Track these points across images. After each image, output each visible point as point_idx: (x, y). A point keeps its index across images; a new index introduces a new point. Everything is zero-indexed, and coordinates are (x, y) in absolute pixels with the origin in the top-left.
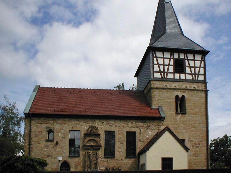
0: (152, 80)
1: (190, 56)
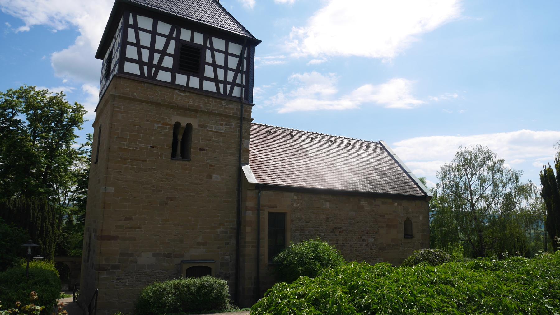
0: (242, 106)
1: (219, 44)
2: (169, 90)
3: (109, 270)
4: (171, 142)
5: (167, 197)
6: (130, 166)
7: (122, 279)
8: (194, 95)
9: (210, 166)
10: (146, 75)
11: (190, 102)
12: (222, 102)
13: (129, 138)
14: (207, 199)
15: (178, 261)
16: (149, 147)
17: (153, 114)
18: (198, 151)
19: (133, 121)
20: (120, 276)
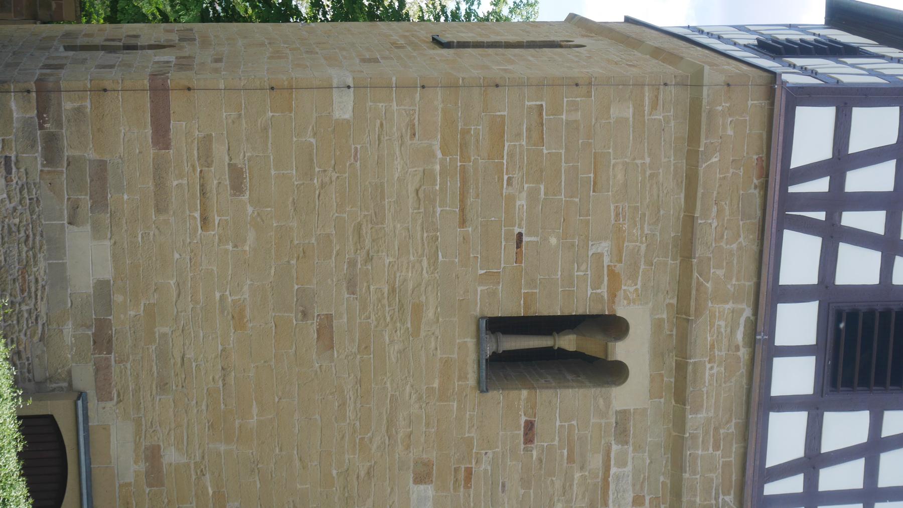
2: (747, 284)
3: (41, 127)
4: (545, 312)
5: (329, 317)
6: (438, 167)
7: (6, 178)
8: (744, 381)
9: (469, 472)
10: (792, 189)
11: (712, 368)
12: (729, 494)
13: (545, 151)
14: (334, 472)
15: (84, 378)
16: (517, 230)
17: (646, 231)
18: (523, 419)
19: (613, 162)
20: (18, 169)
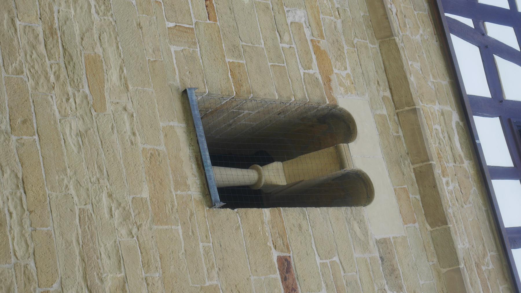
18: (275, 255)
